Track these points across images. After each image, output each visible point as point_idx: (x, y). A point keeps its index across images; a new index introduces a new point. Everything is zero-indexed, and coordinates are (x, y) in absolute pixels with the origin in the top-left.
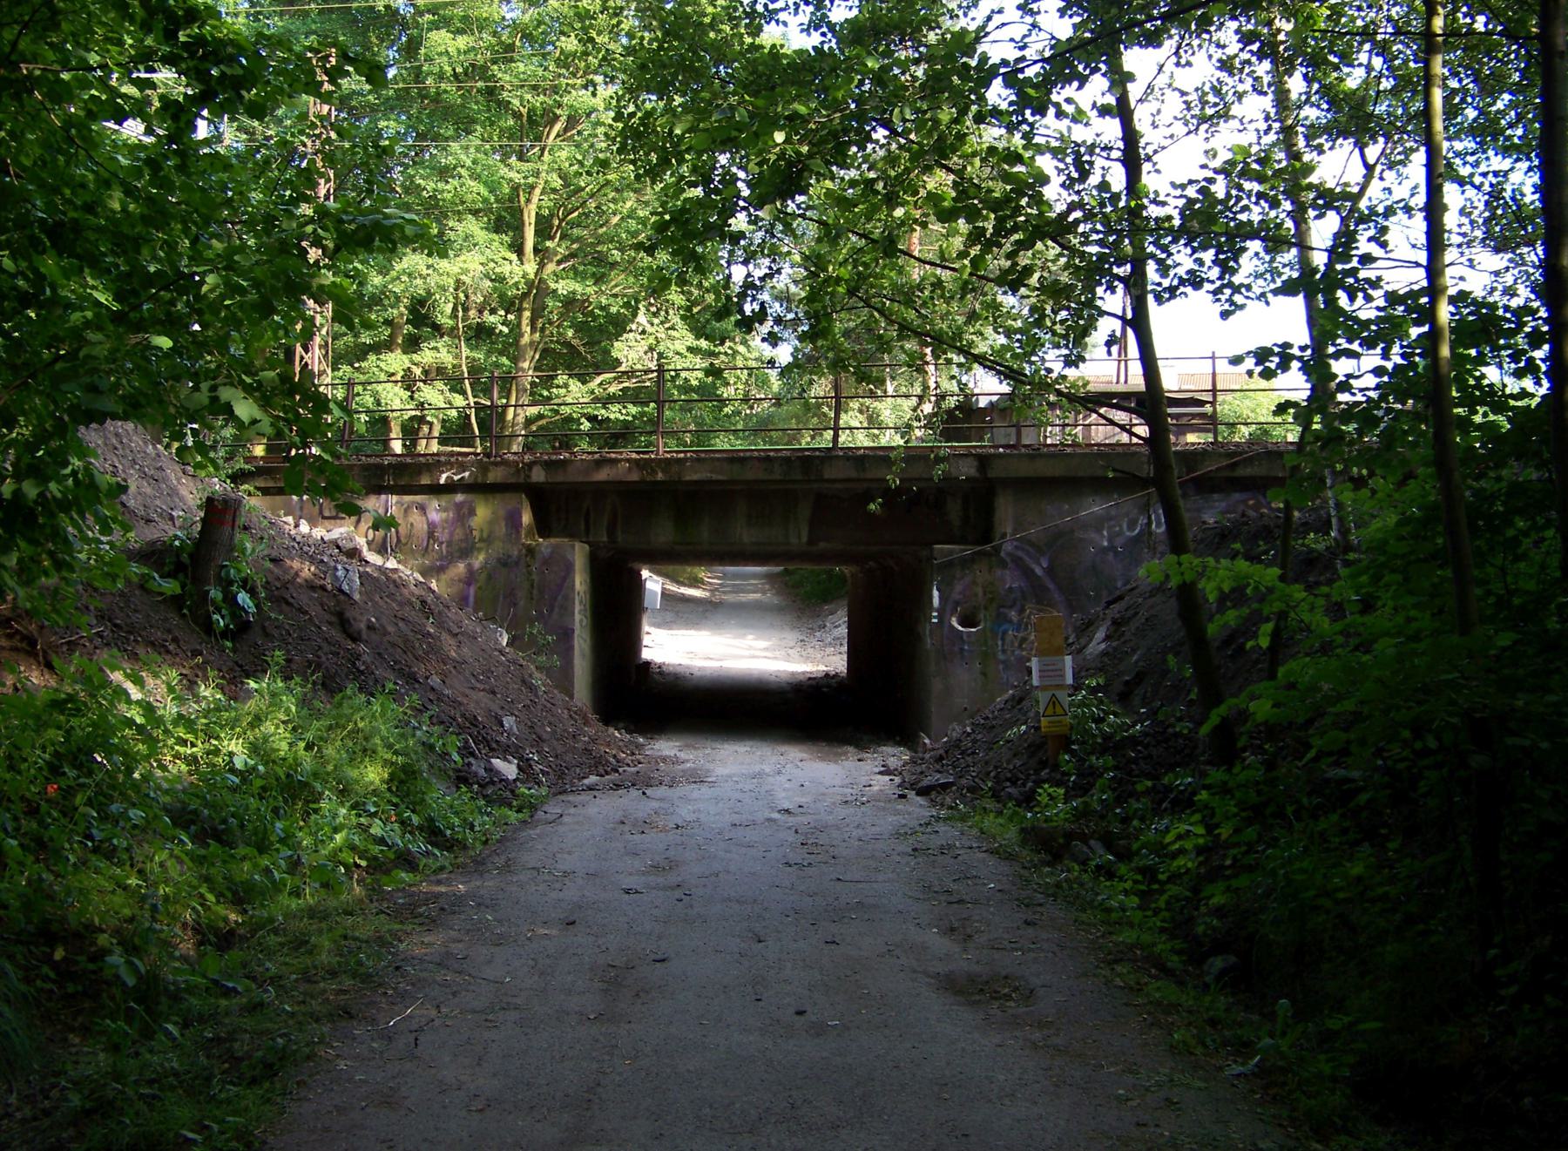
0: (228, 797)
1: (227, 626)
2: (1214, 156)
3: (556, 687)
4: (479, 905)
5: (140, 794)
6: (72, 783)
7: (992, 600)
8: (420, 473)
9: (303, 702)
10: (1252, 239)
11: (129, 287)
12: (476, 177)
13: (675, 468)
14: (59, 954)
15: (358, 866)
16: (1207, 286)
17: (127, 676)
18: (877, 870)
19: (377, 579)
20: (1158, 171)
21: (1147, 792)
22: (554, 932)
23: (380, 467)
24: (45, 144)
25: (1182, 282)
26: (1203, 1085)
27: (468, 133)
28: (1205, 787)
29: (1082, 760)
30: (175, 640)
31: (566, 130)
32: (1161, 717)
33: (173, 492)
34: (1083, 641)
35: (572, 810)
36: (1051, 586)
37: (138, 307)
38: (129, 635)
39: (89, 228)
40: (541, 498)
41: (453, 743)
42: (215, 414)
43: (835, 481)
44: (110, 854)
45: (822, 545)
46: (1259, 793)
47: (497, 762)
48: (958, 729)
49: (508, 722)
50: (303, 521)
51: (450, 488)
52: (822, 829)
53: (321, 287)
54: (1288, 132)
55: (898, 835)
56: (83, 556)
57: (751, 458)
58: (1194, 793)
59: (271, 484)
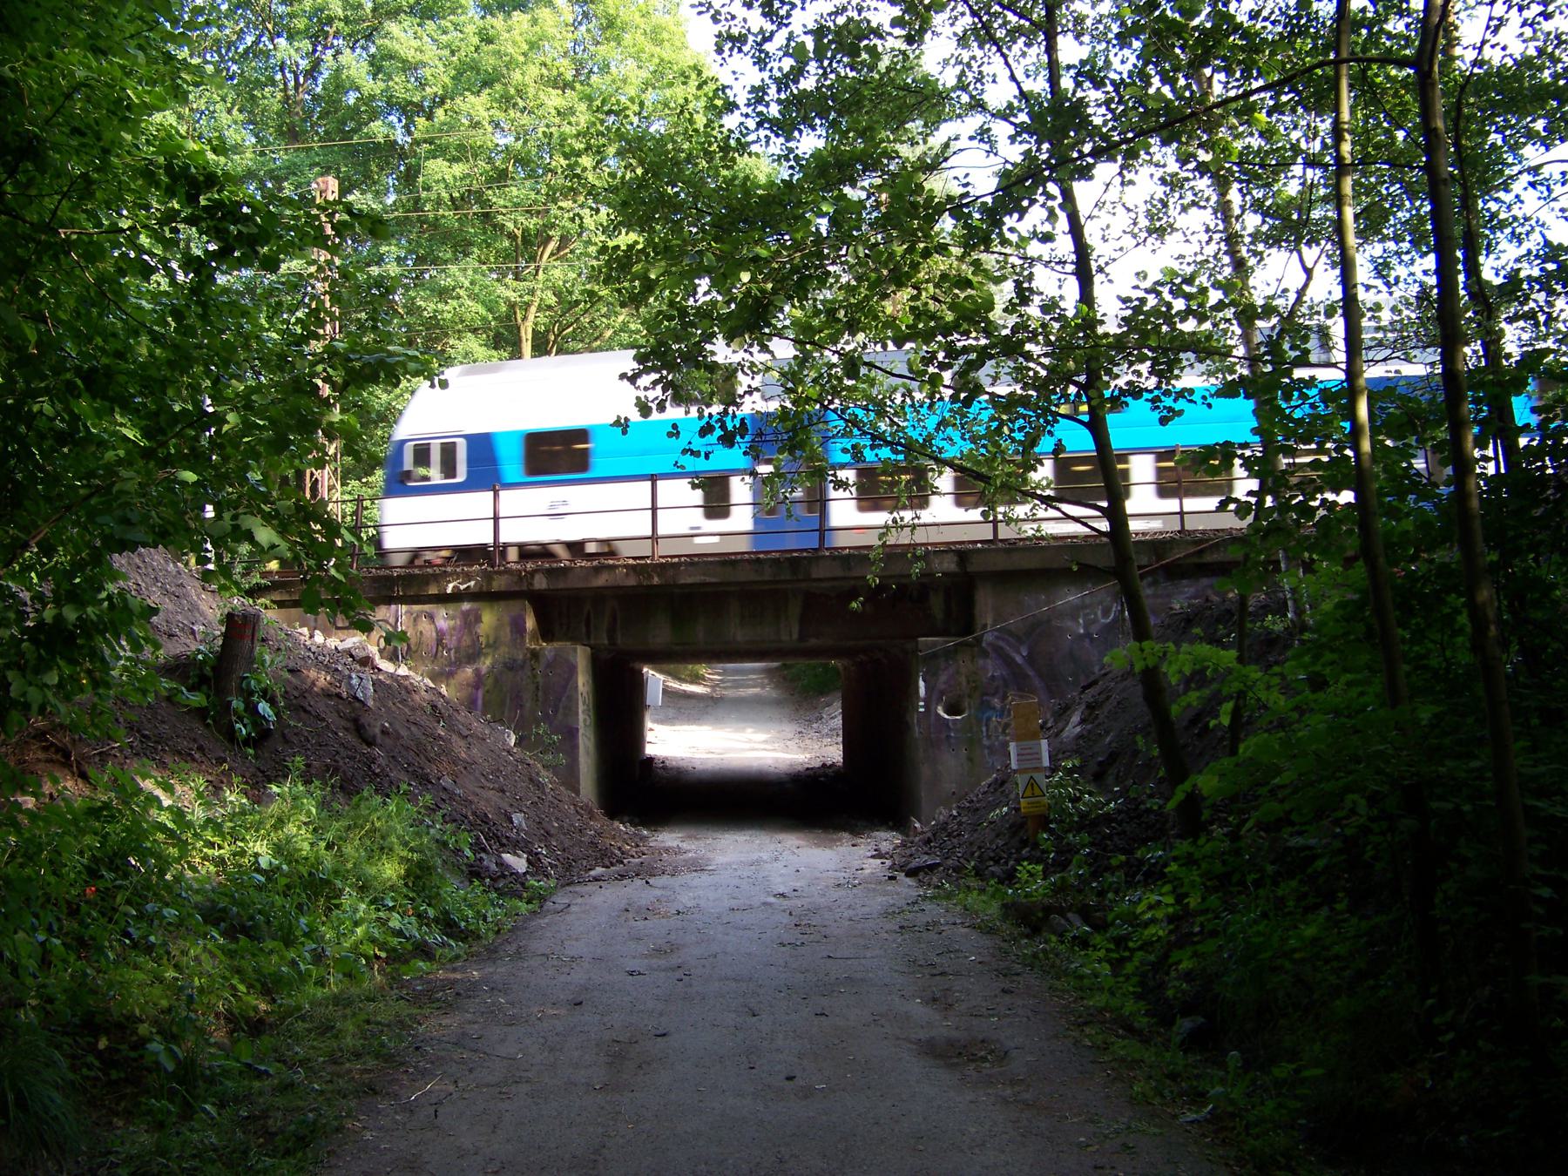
1: (249, 734)
2: (1145, 278)
3: (563, 784)
5: (173, 893)
7: (976, 688)
8: (427, 584)
9: (323, 805)
11: (157, 425)
12: (474, 297)
13: (671, 572)
14: (103, 1043)
16: (1146, 396)
17: (158, 784)
19: (389, 687)
20: (1110, 281)
22: (563, 1012)
23: (389, 578)
25: (1122, 392)
26: (1157, 1130)
27: (466, 255)
28: (1175, 859)
29: (1059, 838)
30: (201, 749)
31: (559, 249)
32: (1132, 795)
33: (194, 608)
34: (1060, 725)
35: (580, 900)
36: (1031, 673)
37: (164, 444)
38: (156, 746)
39: (120, 372)
41: (466, 839)
42: (238, 541)
43: (820, 580)
46: (1224, 863)
47: (507, 857)
49: (518, 818)
51: (457, 597)
52: (815, 910)
53: (331, 424)
54: (1232, 240)
55: (887, 914)
57: (742, 560)
58: (1166, 865)
59: (286, 597)
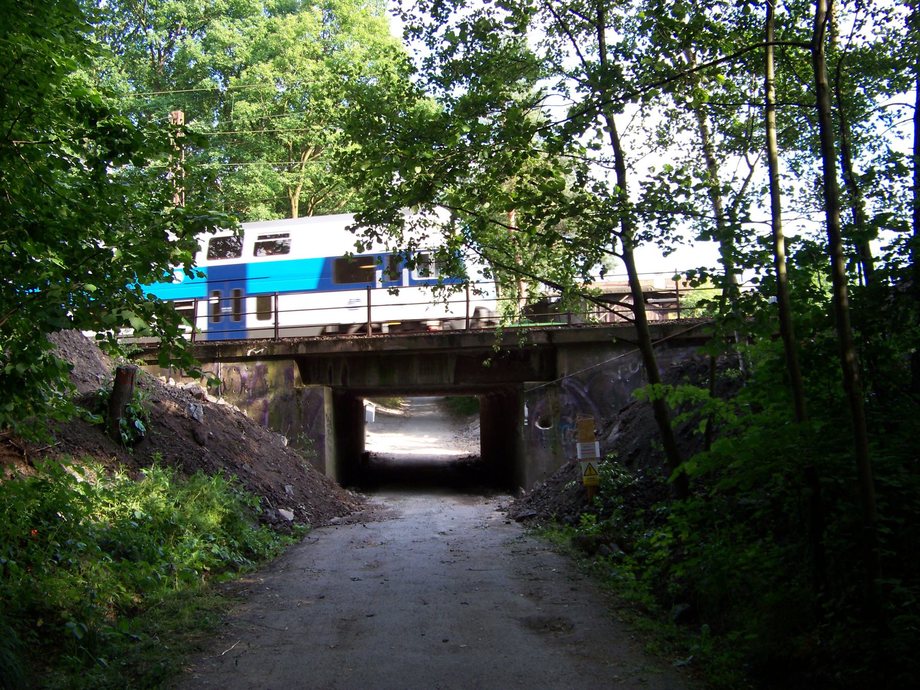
0: (132, 534)
1: (129, 439)
3: (316, 468)
4: (272, 589)
5: (84, 533)
6: (45, 529)
8: (236, 350)
9: (173, 481)
10: (824, 162)
11: (73, 257)
12: (264, 182)
14: (40, 623)
15: (205, 570)
17: (75, 468)
18: (491, 564)
19: (213, 411)
21: (642, 515)
22: (313, 602)
24: (27, 183)
25: (641, 238)
27: (260, 157)
28: (673, 511)
29: (606, 499)
30: (101, 448)
31: (314, 154)
32: (648, 474)
33: (98, 365)
34: (607, 433)
35: (324, 536)
36: (590, 403)
38: (75, 444)
40: (304, 363)
41: (257, 500)
43: (466, 348)
44: (68, 566)
45: (462, 384)
46: (702, 514)
47: (282, 511)
48: (539, 484)
49: (288, 488)
50: (171, 379)
51: (253, 358)
52: (462, 542)
54: (707, 148)
55: (505, 544)
56: (49, 403)
58: (668, 515)
59: (153, 358)
